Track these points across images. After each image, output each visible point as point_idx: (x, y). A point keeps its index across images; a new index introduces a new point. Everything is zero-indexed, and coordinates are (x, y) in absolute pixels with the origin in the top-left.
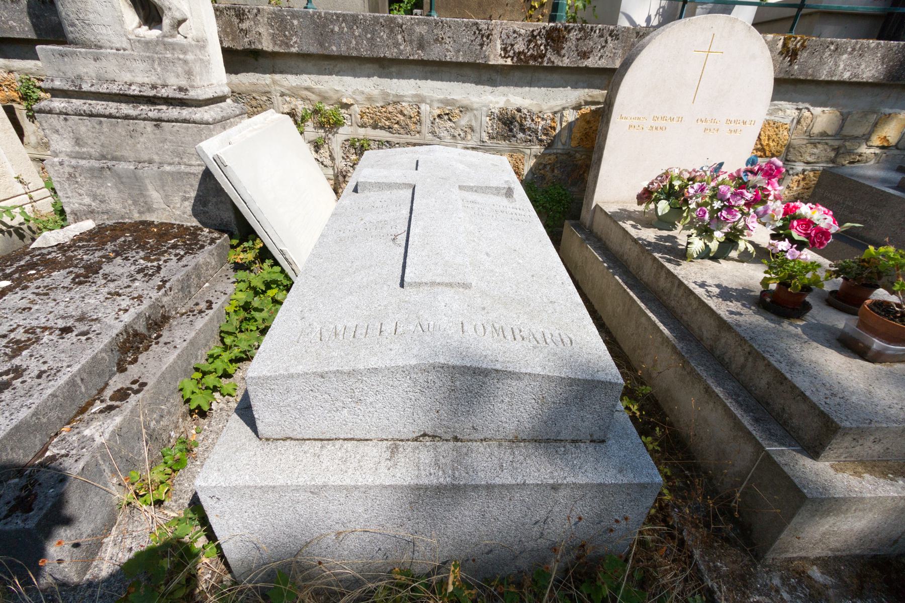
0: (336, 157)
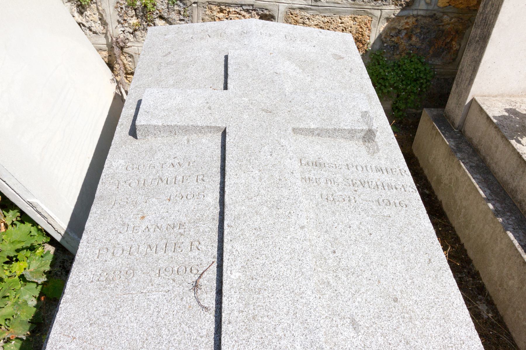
0: (108, 21)
